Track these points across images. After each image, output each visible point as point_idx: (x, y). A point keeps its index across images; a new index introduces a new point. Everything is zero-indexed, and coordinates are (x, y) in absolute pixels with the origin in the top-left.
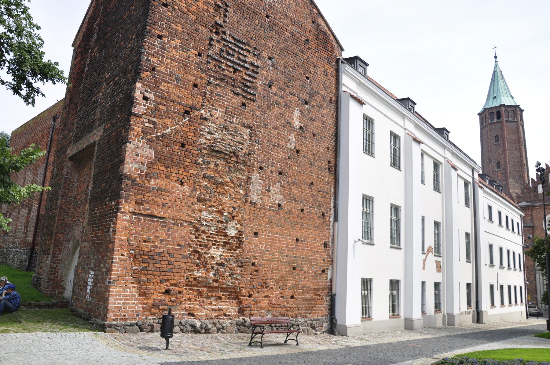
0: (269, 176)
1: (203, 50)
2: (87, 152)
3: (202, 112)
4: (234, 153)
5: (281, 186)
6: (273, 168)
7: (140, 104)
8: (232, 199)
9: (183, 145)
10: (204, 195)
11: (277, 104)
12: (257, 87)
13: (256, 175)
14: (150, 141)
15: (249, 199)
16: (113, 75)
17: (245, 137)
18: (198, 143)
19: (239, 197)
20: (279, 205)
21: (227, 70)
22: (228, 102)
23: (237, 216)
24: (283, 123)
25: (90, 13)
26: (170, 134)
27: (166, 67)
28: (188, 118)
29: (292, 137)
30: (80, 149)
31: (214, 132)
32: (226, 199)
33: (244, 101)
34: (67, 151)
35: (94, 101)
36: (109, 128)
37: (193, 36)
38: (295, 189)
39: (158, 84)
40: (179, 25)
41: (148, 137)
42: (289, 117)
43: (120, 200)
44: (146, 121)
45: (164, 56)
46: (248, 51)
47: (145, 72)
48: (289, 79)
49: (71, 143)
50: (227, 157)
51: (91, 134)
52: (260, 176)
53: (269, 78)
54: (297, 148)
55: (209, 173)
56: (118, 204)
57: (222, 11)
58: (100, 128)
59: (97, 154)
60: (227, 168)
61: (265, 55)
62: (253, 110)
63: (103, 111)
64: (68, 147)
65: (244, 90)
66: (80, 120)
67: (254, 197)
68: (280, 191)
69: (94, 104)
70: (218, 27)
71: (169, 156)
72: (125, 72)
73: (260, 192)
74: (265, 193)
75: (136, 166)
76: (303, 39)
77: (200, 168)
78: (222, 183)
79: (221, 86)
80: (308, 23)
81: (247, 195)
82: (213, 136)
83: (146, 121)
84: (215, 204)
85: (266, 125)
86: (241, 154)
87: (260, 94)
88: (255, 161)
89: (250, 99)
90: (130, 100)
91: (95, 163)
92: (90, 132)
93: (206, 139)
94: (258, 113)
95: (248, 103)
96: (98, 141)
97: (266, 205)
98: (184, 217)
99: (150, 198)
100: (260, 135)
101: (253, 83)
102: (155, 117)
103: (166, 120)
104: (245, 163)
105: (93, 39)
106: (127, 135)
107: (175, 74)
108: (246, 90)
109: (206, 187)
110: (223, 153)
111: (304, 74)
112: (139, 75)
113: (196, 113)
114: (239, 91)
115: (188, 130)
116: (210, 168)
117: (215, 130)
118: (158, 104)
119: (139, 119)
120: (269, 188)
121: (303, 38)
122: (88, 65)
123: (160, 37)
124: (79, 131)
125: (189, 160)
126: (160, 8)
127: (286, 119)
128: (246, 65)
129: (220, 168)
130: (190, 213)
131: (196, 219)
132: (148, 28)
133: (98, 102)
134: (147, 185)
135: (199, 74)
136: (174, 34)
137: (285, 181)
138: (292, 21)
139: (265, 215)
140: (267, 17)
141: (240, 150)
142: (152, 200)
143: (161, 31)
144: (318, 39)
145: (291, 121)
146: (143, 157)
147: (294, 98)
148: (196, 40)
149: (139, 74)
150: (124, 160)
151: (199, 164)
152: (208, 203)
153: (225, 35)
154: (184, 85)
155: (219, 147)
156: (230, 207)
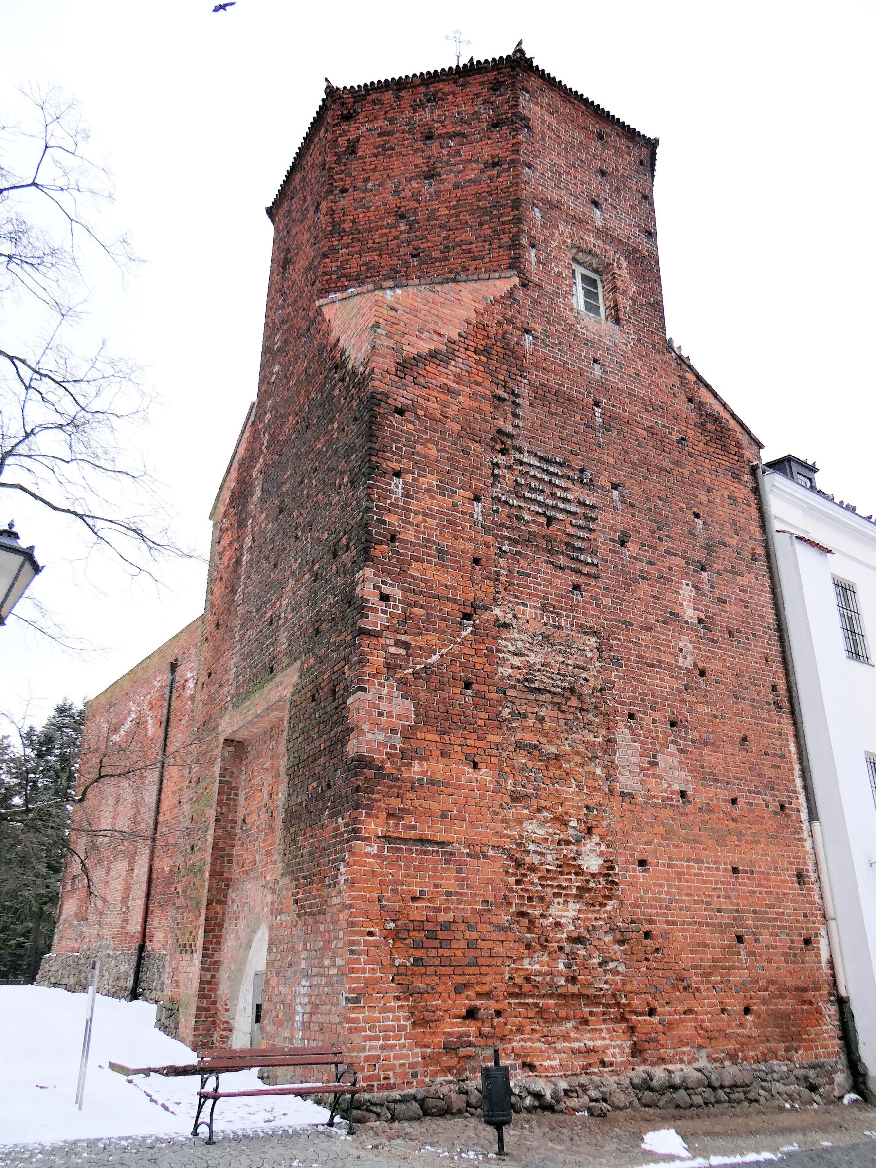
0: (650, 731)
1: (482, 489)
3: (497, 611)
4: (572, 690)
6: (657, 715)
7: (375, 610)
12: (597, 547)
13: (623, 734)
15: (618, 786)
20: (683, 794)
21: (534, 522)
22: (544, 586)
27: (416, 531)
29: (684, 643)
36: (312, 667)
38: (709, 755)
40: (430, 446)
45: (409, 510)
52: (633, 734)
61: (603, 481)
63: (292, 635)
67: (627, 781)
68: (679, 763)
70: (505, 439)
80: (680, 405)
84: (549, 804)
86: (586, 690)
88: (617, 702)
89: (589, 575)
94: (607, 601)
100: (618, 645)
103: (428, 637)
105: (255, 499)
109: (524, 768)
113: (486, 615)
114: (562, 561)
115: (473, 652)
120: (655, 757)
125: (483, 715)
127: (667, 607)
128: (570, 508)
136: (424, 466)
137: (685, 739)
138: (649, 406)
141: (583, 683)
144: (704, 431)
146: (392, 716)
154: (455, 562)
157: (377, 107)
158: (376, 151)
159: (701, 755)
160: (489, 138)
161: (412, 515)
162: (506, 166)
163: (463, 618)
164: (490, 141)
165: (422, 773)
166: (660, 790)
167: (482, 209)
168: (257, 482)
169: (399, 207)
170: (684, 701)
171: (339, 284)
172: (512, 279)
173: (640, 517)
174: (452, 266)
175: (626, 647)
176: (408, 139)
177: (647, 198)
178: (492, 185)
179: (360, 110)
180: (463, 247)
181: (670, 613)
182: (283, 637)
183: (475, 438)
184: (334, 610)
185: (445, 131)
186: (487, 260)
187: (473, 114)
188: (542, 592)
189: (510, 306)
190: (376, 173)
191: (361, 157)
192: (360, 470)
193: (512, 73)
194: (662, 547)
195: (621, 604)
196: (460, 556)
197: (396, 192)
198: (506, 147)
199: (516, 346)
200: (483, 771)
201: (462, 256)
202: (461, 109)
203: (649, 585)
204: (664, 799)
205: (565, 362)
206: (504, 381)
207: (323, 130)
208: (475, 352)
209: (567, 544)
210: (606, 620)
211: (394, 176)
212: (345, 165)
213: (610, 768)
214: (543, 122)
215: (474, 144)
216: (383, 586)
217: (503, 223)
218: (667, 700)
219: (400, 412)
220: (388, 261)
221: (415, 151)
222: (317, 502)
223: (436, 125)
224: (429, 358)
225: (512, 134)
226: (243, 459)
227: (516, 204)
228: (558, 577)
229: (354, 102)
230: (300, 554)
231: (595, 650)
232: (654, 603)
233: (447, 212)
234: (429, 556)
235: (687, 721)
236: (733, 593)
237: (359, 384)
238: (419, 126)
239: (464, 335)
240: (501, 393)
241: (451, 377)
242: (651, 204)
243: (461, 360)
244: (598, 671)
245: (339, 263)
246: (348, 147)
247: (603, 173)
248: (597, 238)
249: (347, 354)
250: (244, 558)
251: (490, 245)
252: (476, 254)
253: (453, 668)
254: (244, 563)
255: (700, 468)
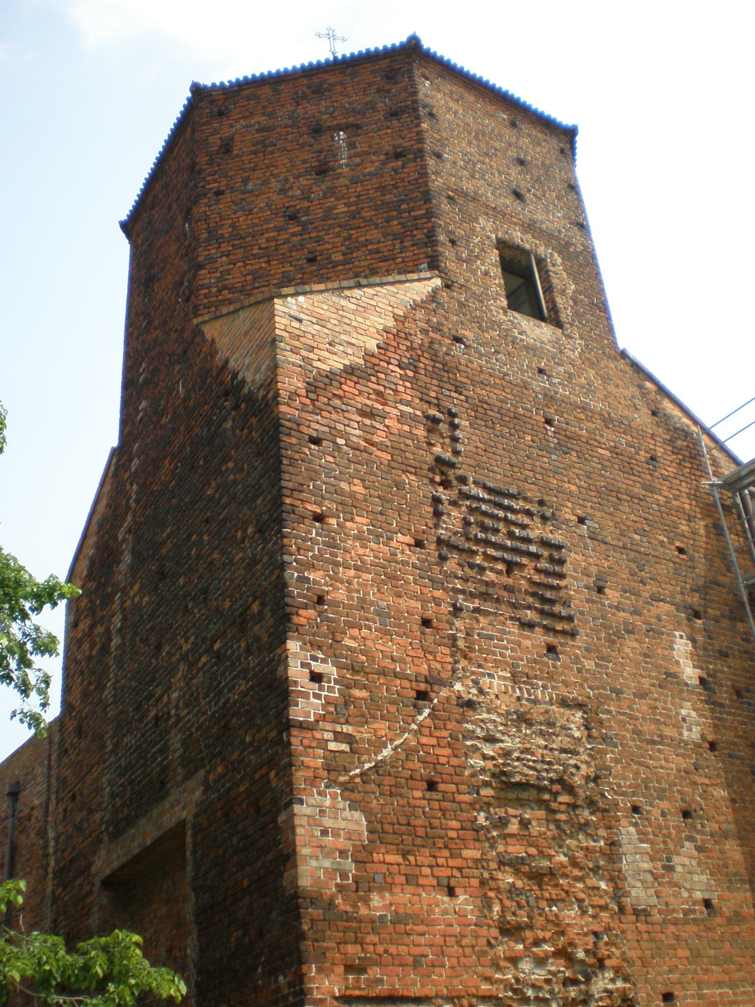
0: (660, 827)
1: (424, 532)
2: (163, 855)
3: (458, 686)
4: (561, 781)
5: (699, 849)
6: (665, 805)
7: (305, 695)
8: (584, 912)
9: (432, 786)
10: (514, 914)
11: (628, 632)
12: (570, 597)
13: (628, 833)
14: (347, 788)
15: (627, 901)
16: (204, 640)
17: (577, 734)
18: (467, 773)
19: (602, 902)
20: (707, 903)
21: (492, 569)
22: (512, 650)
23: (609, 957)
24: (656, 678)
25: (101, 508)
26: (394, 760)
27: (349, 590)
28: (427, 711)
29: (686, 711)
30: (136, 852)
31: (498, 735)
32: (570, 914)
33: (551, 639)
34: (90, 865)
35: (157, 718)
36: (221, 776)
37: (392, 501)
39: (338, 636)
40: (356, 481)
41: (342, 779)
42: (664, 658)
43: (305, 968)
44: (328, 736)
45: (336, 564)
46: (528, 513)
47: (301, 612)
48: (640, 560)
49: (101, 841)
50: (547, 797)
51: (167, 804)
52: (639, 832)
53: (594, 570)
54: (710, 737)
55: (510, 849)
56: (300, 978)
57: (443, 427)
58: (190, 784)
59: (194, 853)
60: (552, 827)
61: (567, 514)
62: (577, 660)
63: (190, 736)
64: (95, 853)
65: (542, 612)
66: (121, 775)
67: (638, 893)
68: (699, 864)
69: (156, 725)
70: (444, 469)
71: (403, 820)
72: (242, 622)
73: (649, 878)
74: (663, 876)
75: (327, 864)
76: (643, 459)
77: (488, 839)
78: (551, 873)
79: (486, 613)
80: (642, 418)
81: (618, 894)
82: (498, 745)
83: (328, 736)
84: (548, 935)
85: (619, 692)
86: (578, 780)
87: (582, 613)
88: (616, 793)
89: (564, 633)
90: (279, 691)
91: (195, 878)
92: (160, 799)
93: (485, 757)
94: (589, 664)
95: (562, 644)
96: (190, 818)
97: (674, 911)
98: (477, 988)
99: (380, 949)
100: (609, 720)
101: (558, 588)
102: (347, 722)
103: (376, 726)
104: (591, 803)
105: (123, 567)
106: (290, 784)
107: (372, 603)
108: (549, 612)
109: (512, 890)
110: (533, 786)
111: (671, 543)
112: (290, 620)
113: (444, 693)
114: (530, 615)
115: (433, 741)
116: (512, 836)
117: (501, 728)
118: (349, 687)
119: (309, 735)
120: (669, 860)
121: (643, 456)
122: (120, 630)
123: (319, 518)
124: (123, 806)
125: (454, 824)
126: (307, 451)
127: (661, 666)
128: (533, 549)
129: (536, 829)
130: (489, 972)
131: (508, 986)
132: (288, 501)
133: (169, 717)
134: (363, 911)
135: (429, 592)
136: (350, 506)
137: (702, 833)
138: (607, 421)
139: (677, 938)
140: (549, 422)
141: (573, 770)
142: (386, 951)
143: (320, 505)
144: (676, 451)
145: (673, 669)
146: (339, 835)
147: (664, 607)
148: (402, 510)
149: (287, 617)
150: (294, 852)
151: (482, 827)
152: (528, 934)
153: (466, 485)
154: (400, 626)
155: (522, 772)
156: (586, 935)
157: (253, 102)
158: (254, 148)
159: (722, 852)
160: (388, 128)
161: (341, 569)
162: (412, 156)
163: (417, 698)
164: (389, 131)
165: (385, 907)
166: (679, 902)
167: (387, 203)
168: (124, 546)
169: (288, 208)
170: (694, 784)
171: (220, 298)
172: (433, 280)
173: (615, 556)
174: (359, 270)
175: (620, 721)
176: (292, 134)
177: (573, 188)
178: (397, 177)
179: (232, 107)
180: (369, 247)
181: (665, 673)
182: (175, 740)
183: (409, 468)
184: (247, 699)
185: (335, 123)
186: (400, 260)
187: (367, 103)
188: (510, 657)
189: (434, 311)
190: (257, 172)
191: (237, 156)
192: (271, 516)
193: (407, 60)
194: (647, 590)
195: (607, 667)
196: (405, 618)
197: (283, 191)
198: (409, 136)
199: (447, 358)
200: (462, 898)
201: (368, 257)
202: (351, 99)
203: (637, 640)
204: (686, 913)
205: (506, 374)
206: (437, 398)
207: (189, 131)
208: (399, 366)
209: (534, 595)
210: (591, 688)
211: (278, 175)
212: (218, 165)
213: (616, 879)
214: (449, 109)
215: (370, 135)
216: (313, 663)
217: (415, 218)
218: (676, 785)
219: (316, 441)
220: (277, 269)
221: (302, 146)
222: (211, 563)
223: (324, 117)
224: (344, 375)
225: (415, 122)
226: (399, 273)
227: (427, 197)
228: (528, 638)
229: (226, 99)
230: (192, 631)
231: (582, 728)
232: (646, 662)
233: (346, 209)
234: (368, 620)
235: (702, 809)
236: (735, 643)
237: (260, 411)
238: (303, 119)
239: (382, 345)
240: (432, 412)
241: (373, 396)
242: (578, 194)
243: (383, 376)
244: (589, 755)
245: (218, 275)
246: (221, 147)
247: (521, 162)
248: (525, 232)
249: (240, 377)
250: (113, 644)
251: (402, 242)
252: (386, 254)
253: (410, 765)
254: (113, 649)
255: (676, 492)
